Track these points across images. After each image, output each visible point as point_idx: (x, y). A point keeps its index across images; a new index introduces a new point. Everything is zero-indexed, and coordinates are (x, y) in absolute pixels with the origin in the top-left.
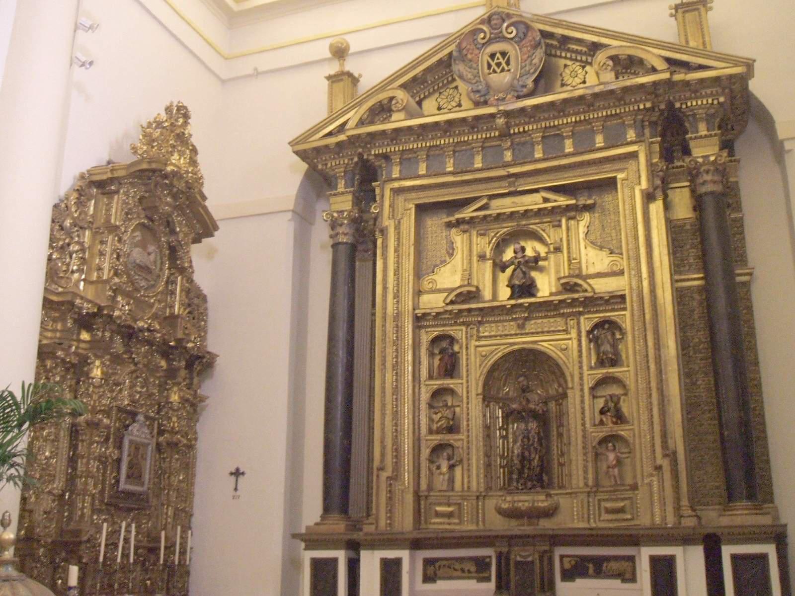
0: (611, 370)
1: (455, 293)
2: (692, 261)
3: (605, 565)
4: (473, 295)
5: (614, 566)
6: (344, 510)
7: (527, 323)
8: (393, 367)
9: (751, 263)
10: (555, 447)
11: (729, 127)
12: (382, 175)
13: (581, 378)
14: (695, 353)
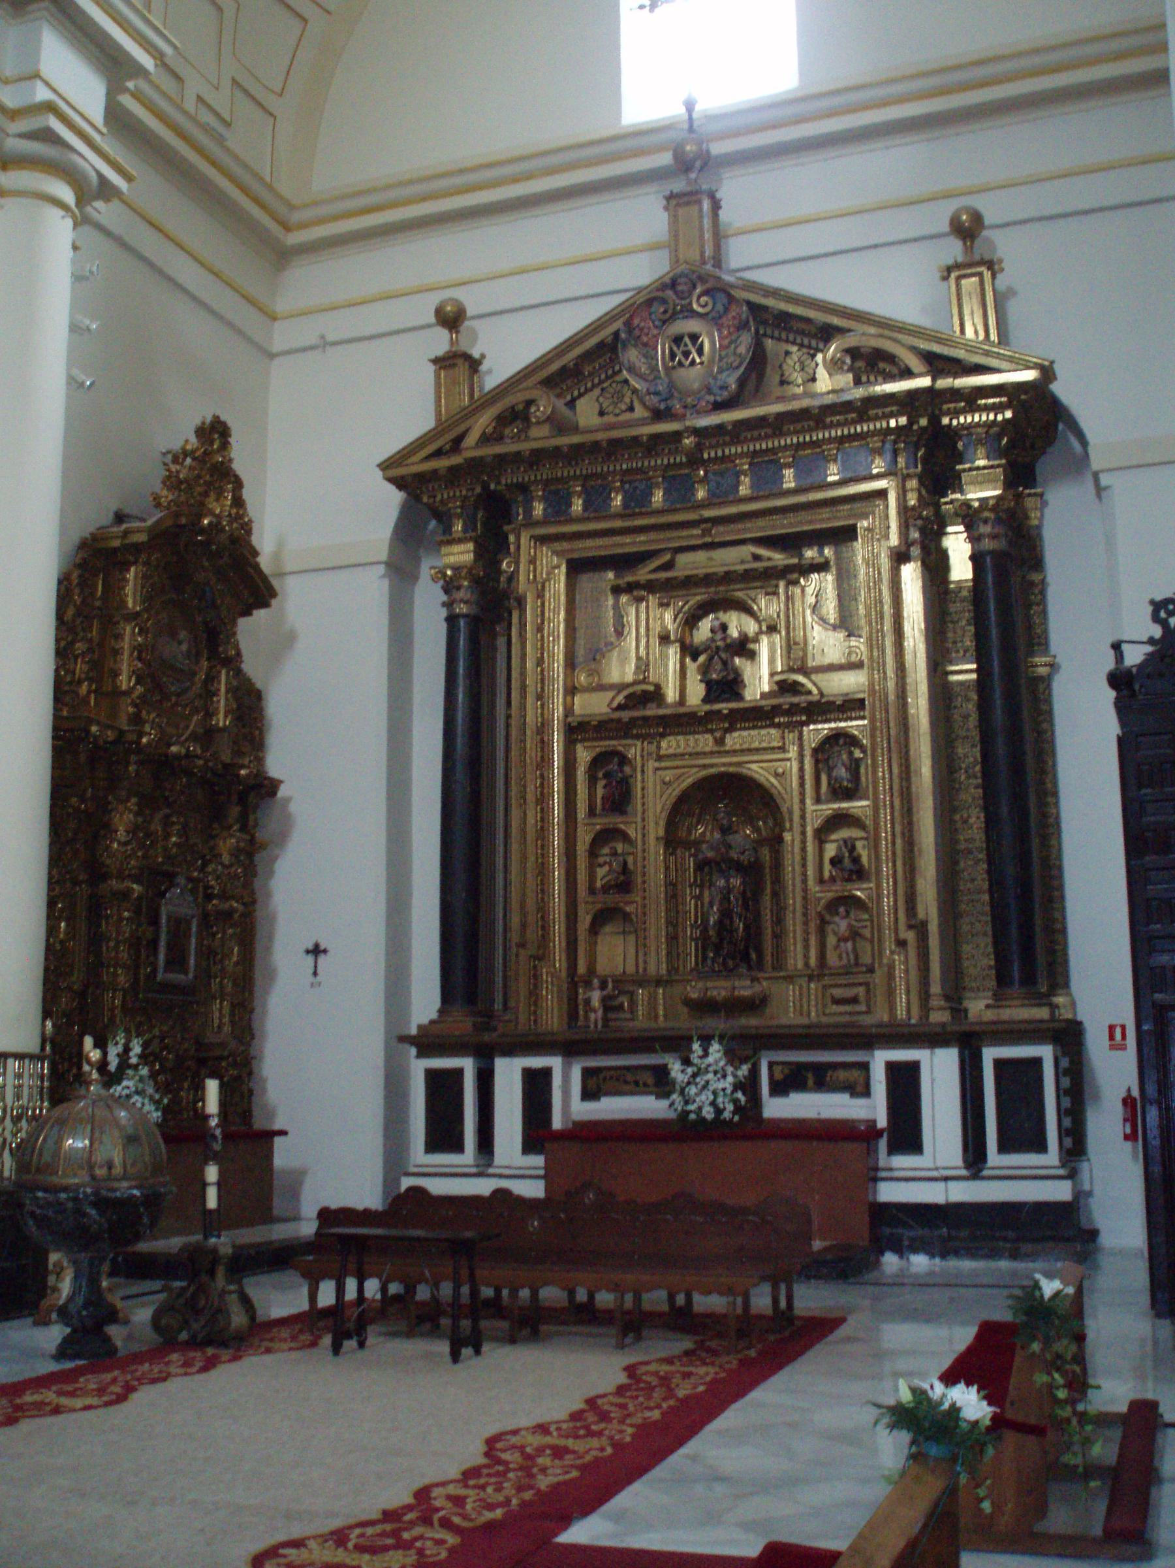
0: (844, 805)
1: (625, 693)
2: (969, 643)
3: (830, 1073)
4: (656, 695)
5: (842, 1075)
6: (471, 999)
7: (728, 736)
8: (537, 800)
9: (1054, 648)
10: (768, 911)
11: (1028, 444)
12: (518, 515)
13: (803, 817)
14: (968, 777)
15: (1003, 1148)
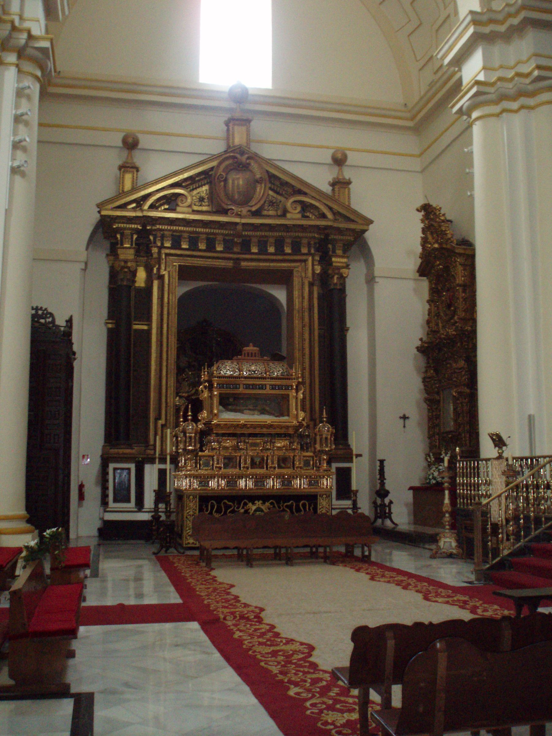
15: (115, 500)
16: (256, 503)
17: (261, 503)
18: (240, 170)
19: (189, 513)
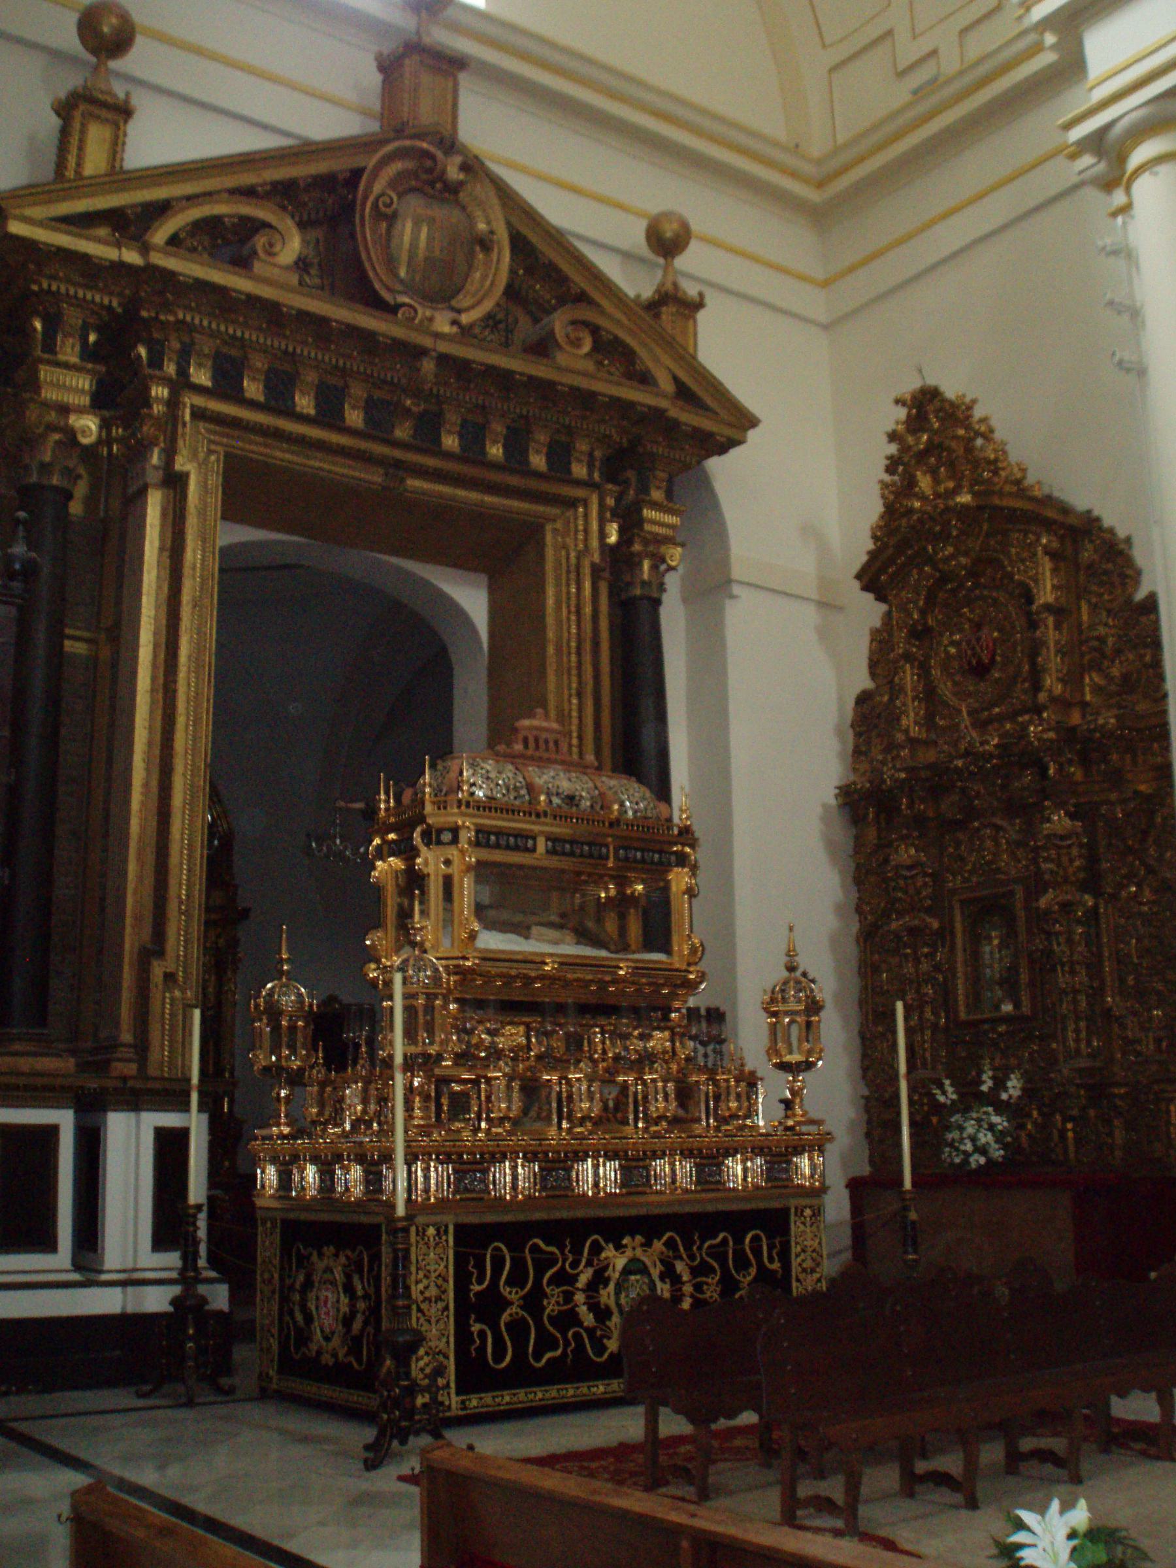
16: (625, 1246)
17: (642, 1245)
18: (432, 197)
19: (427, 1294)
